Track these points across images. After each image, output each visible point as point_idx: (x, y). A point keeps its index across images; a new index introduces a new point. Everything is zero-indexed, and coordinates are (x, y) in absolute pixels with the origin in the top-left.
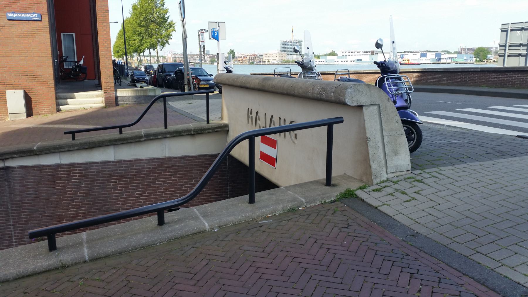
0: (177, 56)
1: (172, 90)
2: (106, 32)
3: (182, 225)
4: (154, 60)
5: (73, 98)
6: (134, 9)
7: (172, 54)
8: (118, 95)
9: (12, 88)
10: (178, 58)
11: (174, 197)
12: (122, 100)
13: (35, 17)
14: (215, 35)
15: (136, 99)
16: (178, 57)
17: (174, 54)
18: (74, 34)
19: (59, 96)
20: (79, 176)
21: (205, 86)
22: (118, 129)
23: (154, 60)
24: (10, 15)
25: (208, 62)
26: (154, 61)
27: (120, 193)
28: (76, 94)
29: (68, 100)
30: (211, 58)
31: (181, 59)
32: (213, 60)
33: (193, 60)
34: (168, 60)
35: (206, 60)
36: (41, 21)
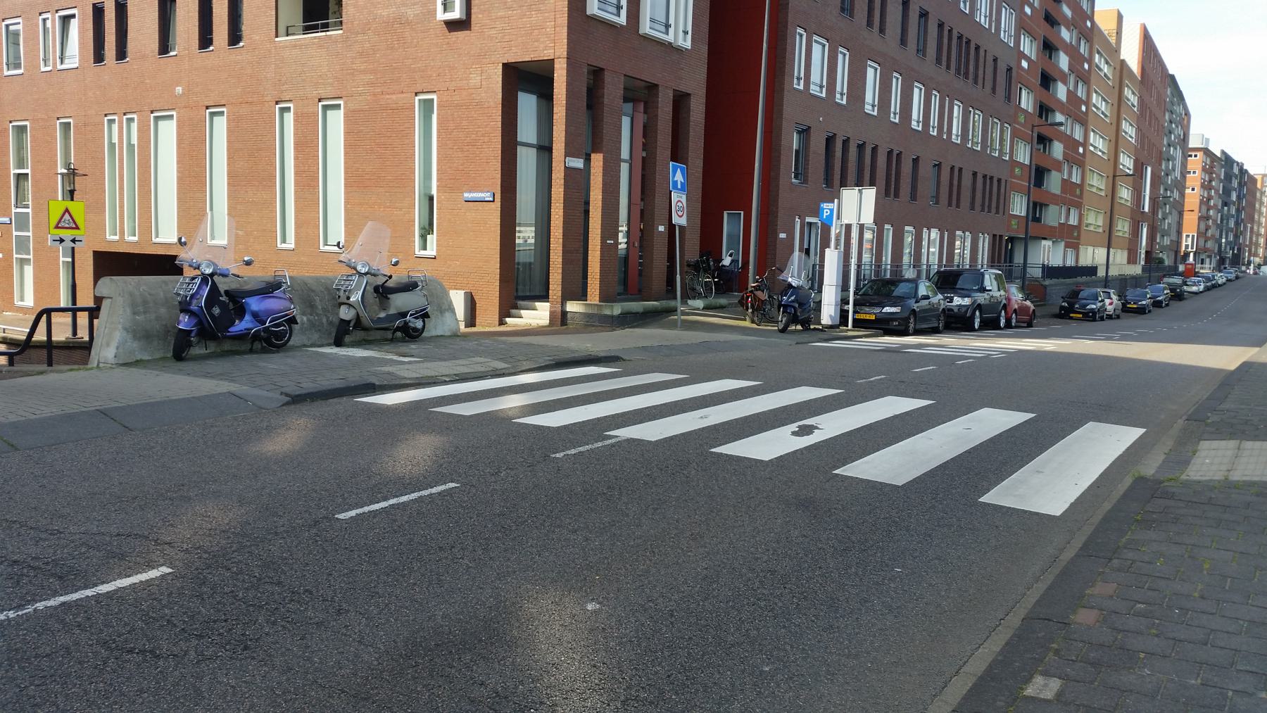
2: (557, 216)
3: (1193, 682)
5: (534, 309)
8: (567, 310)
9: (460, 287)
12: (572, 319)
13: (488, 196)
14: (825, 214)
15: (587, 319)
18: (742, 212)
19: (520, 304)
21: (868, 318)
22: (87, 313)
24: (467, 195)
28: (537, 304)
29: (522, 312)
36: (493, 201)
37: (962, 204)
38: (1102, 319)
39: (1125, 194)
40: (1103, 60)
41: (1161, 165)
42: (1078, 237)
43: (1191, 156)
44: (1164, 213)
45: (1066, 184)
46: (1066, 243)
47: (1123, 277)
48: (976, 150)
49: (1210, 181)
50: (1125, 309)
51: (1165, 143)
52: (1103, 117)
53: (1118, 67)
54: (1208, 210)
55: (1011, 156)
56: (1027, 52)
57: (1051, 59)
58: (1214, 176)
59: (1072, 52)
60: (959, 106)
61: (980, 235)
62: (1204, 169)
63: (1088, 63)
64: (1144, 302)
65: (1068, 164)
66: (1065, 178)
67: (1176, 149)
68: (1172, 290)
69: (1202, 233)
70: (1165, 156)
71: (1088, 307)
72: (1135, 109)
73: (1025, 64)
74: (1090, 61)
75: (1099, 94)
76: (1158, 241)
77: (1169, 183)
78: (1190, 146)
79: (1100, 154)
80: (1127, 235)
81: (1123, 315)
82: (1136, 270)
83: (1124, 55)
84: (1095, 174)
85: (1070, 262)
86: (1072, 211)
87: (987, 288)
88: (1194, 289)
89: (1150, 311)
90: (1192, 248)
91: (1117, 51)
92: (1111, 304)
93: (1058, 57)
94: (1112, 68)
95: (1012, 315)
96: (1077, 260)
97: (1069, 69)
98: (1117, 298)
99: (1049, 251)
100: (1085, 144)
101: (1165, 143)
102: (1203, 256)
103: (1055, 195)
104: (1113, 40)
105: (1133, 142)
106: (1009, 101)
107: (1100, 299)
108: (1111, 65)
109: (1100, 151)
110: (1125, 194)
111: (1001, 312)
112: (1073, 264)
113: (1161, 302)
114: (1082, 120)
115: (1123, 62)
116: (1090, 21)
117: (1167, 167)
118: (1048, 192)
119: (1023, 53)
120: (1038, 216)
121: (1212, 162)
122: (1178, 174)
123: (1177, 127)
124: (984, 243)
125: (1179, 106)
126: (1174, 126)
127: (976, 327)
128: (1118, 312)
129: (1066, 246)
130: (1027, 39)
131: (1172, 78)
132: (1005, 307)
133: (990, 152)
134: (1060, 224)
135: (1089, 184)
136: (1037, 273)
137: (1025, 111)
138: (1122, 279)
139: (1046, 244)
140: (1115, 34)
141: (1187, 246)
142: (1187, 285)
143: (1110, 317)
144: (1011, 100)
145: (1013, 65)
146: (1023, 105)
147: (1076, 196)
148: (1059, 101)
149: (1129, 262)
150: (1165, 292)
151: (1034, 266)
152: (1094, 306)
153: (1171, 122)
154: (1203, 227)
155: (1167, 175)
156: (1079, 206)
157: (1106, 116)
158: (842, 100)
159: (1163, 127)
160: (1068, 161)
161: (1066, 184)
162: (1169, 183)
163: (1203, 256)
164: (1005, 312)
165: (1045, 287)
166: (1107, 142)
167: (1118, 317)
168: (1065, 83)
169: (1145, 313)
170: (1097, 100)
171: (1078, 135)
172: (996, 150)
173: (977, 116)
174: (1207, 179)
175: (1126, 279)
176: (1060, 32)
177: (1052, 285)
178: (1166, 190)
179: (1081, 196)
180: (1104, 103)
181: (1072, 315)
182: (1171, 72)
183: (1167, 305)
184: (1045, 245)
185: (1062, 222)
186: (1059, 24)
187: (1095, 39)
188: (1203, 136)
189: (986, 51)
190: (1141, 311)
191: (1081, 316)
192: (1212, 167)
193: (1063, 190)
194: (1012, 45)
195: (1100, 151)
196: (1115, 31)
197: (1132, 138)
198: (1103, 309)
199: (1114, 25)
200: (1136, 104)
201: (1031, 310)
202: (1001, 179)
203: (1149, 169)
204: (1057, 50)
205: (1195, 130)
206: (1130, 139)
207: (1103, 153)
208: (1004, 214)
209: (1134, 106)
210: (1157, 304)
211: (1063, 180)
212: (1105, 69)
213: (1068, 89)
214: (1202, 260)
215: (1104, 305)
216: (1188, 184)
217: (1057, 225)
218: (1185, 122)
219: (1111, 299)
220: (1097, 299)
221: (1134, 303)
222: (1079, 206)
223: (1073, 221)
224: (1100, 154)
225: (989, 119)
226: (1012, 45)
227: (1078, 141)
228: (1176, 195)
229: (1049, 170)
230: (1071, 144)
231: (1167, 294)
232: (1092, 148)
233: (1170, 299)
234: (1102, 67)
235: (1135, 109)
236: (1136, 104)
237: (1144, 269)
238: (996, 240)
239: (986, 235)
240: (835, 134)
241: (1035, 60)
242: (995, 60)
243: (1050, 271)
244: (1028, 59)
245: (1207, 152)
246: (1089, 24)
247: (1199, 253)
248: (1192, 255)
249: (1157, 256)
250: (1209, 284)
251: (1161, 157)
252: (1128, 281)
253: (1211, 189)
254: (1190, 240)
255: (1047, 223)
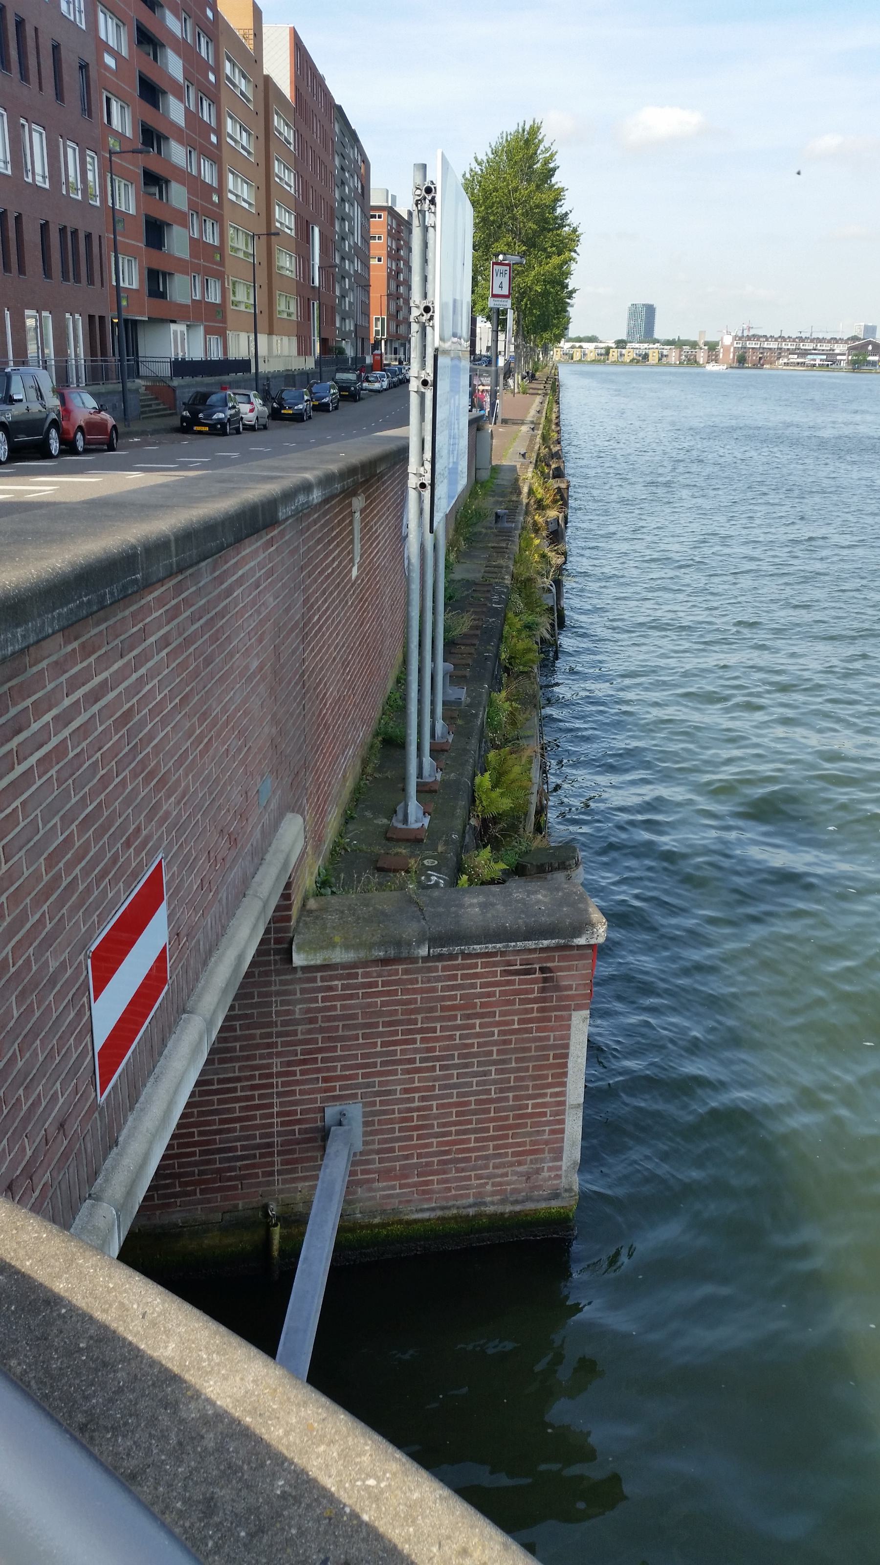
0: (750, 344)
1: (35, 500)
4: (681, 355)
6: (508, 152)
7: (736, 336)
10: (753, 348)
11: (196, 1107)
16: (754, 346)
17: (832, 339)
20: (495, 1129)
23: (681, 355)
25: (843, 364)
26: (680, 359)
27: (449, 1134)
30: (854, 352)
31: (762, 353)
32: (861, 358)
33: (796, 356)
34: (721, 355)
35: (839, 357)
37: (29, 268)
38: (238, 432)
39: (286, 263)
40: (237, 71)
41: (333, 225)
42: (224, 320)
43: (374, 216)
44: (342, 289)
45: (196, 245)
46: (205, 327)
47: (290, 373)
48: (93, 206)
49: (398, 250)
50: (276, 415)
51: (337, 196)
52: (245, 154)
53: (261, 87)
54: (398, 286)
55: (104, 200)
56: (112, 42)
57: (157, 62)
58: (402, 243)
59: (188, 54)
60: (41, 134)
61: (68, 315)
62: (389, 234)
63: (214, 73)
64: (301, 406)
65: (198, 217)
66: (196, 237)
67: (353, 205)
68: (341, 389)
69: (392, 315)
70: (338, 214)
71: (215, 417)
72: (292, 148)
73: (110, 61)
74: (217, 70)
75: (236, 121)
76: (338, 325)
77: (347, 249)
78: (372, 204)
79: (246, 206)
80: (294, 318)
81: (271, 424)
82: (309, 364)
83: (269, 68)
84: (240, 233)
85: (216, 354)
86: (211, 282)
87: (16, 397)
88: (377, 386)
89: (310, 418)
90: (383, 335)
91: (256, 60)
92: (252, 411)
93: (166, 58)
94: (252, 86)
95: (76, 434)
96: (225, 352)
97: (185, 78)
98: (261, 402)
99: (183, 340)
100: (221, 189)
101: (337, 196)
102: (396, 345)
103: (180, 259)
104: (250, 45)
105: (292, 192)
106: (90, 116)
107: (230, 405)
108: (249, 81)
109: (244, 200)
110: (286, 263)
111: (48, 432)
112: (221, 356)
113: (327, 404)
114: (215, 156)
115: (267, 79)
116: (211, 10)
117: (342, 228)
118: (171, 256)
119: (106, 44)
120: (161, 289)
121: (398, 225)
122: (357, 238)
123: (352, 176)
124: (76, 325)
125: (353, 148)
126: (347, 175)
127: (80, 449)
128: (262, 421)
129: (207, 332)
130: (109, 20)
131: (339, 109)
132: (55, 424)
133: (68, 191)
134: (193, 300)
135: (232, 247)
136: (166, 370)
137: (120, 136)
138: (287, 375)
139: (178, 328)
140: (252, 37)
141: (377, 332)
142: (370, 381)
143: (251, 428)
144: (93, 114)
145: (90, 59)
146: (116, 123)
147: (216, 263)
148: (173, 124)
149: (299, 353)
150: (332, 391)
151: (157, 360)
152: (221, 415)
153: (342, 169)
154: (393, 309)
155: (343, 239)
156: (220, 276)
157: (249, 153)
158: (7, 169)
159: (333, 175)
160: (197, 213)
161: (196, 245)
162: (347, 249)
163: (396, 345)
164: (58, 431)
165: (174, 389)
166: (254, 189)
167: (265, 427)
168: (180, 99)
169: (303, 421)
170: (234, 128)
171: (208, 173)
172: (77, 190)
173: (88, 159)
174: (394, 247)
175: (294, 376)
176: (163, 18)
177: (182, 387)
178: (343, 259)
179: (222, 263)
180: (244, 134)
181: (195, 428)
182: (337, 102)
183: (336, 408)
184: (175, 332)
185: (198, 298)
186: (162, 6)
187: (222, 39)
188: (387, 191)
189: (36, 29)
190: (298, 418)
191: (207, 429)
192: (399, 232)
193: (194, 253)
194: (83, 27)
195: (244, 200)
196: (252, 32)
197: (290, 187)
198: (237, 417)
199: (249, 23)
200: (292, 141)
201: (110, 426)
202: (77, 230)
203: (316, 230)
204: (163, 46)
205: (376, 182)
206: (288, 189)
207: (250, 204)
208: (102, 285)
209: (290, 143)
210: (322, 408)
211: (191, 238)
212: (243, 85)
213: (187, 110)
214: (396, 349)
215: (238, 413)
216: (373, 252)
217: (189, 302)
218: (362, 171)
219: (252, 404)
220: (227, 405)
221: (290, 408)
222: (220, 276)
223: (214, 296)
224: (246, 206)
225: (58, 141)
226: (83, 27)
227: (211, 186)
228: (358, 265)
229: (169, 225)
230: (195, 184)
231: (334, 394)
232: (231, 197)
233: (339, 400)
234: (237, 82)
235: (292, 148)
236: (292, 141)
237: (318, 363)
238: (95, 324)
239: (77, 316)
240: (5, 210)
241: (127, 57)
242: (56, 48)
243: (182, 367)
244: (116, 55)
245: (391, 212)
246: (210, 14)
247: (391, 341)
248: (383, 342)
249: (338, 345)
250: (395, 379)
251: (333, 215)
252: (297, 377)
253: (399, 260)
254: (379, 323)
255: (173, 299)
